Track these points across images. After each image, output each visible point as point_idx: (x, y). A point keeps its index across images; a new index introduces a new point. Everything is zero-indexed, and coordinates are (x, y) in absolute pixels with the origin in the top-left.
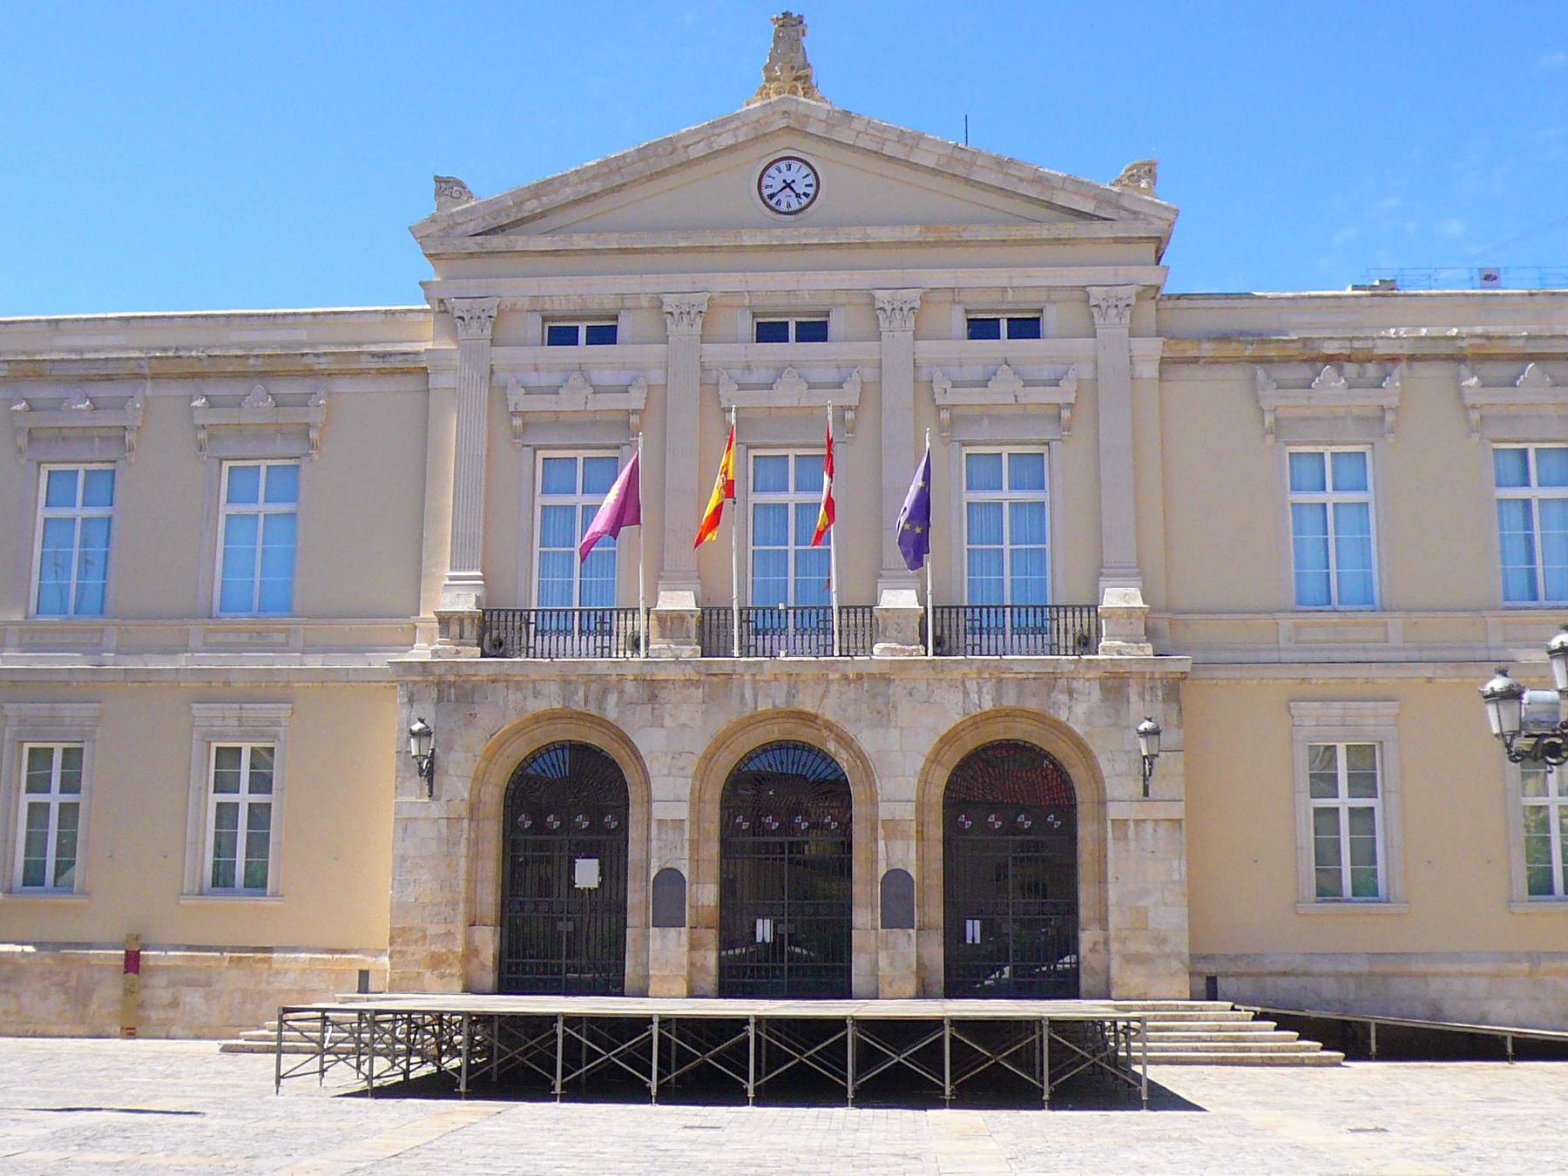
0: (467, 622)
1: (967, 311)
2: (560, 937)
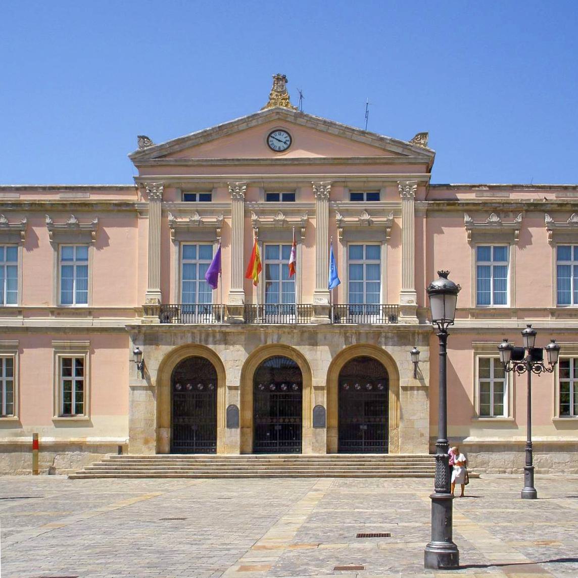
0: (155, 310)
1: (350, 191)
2: (276, 431)
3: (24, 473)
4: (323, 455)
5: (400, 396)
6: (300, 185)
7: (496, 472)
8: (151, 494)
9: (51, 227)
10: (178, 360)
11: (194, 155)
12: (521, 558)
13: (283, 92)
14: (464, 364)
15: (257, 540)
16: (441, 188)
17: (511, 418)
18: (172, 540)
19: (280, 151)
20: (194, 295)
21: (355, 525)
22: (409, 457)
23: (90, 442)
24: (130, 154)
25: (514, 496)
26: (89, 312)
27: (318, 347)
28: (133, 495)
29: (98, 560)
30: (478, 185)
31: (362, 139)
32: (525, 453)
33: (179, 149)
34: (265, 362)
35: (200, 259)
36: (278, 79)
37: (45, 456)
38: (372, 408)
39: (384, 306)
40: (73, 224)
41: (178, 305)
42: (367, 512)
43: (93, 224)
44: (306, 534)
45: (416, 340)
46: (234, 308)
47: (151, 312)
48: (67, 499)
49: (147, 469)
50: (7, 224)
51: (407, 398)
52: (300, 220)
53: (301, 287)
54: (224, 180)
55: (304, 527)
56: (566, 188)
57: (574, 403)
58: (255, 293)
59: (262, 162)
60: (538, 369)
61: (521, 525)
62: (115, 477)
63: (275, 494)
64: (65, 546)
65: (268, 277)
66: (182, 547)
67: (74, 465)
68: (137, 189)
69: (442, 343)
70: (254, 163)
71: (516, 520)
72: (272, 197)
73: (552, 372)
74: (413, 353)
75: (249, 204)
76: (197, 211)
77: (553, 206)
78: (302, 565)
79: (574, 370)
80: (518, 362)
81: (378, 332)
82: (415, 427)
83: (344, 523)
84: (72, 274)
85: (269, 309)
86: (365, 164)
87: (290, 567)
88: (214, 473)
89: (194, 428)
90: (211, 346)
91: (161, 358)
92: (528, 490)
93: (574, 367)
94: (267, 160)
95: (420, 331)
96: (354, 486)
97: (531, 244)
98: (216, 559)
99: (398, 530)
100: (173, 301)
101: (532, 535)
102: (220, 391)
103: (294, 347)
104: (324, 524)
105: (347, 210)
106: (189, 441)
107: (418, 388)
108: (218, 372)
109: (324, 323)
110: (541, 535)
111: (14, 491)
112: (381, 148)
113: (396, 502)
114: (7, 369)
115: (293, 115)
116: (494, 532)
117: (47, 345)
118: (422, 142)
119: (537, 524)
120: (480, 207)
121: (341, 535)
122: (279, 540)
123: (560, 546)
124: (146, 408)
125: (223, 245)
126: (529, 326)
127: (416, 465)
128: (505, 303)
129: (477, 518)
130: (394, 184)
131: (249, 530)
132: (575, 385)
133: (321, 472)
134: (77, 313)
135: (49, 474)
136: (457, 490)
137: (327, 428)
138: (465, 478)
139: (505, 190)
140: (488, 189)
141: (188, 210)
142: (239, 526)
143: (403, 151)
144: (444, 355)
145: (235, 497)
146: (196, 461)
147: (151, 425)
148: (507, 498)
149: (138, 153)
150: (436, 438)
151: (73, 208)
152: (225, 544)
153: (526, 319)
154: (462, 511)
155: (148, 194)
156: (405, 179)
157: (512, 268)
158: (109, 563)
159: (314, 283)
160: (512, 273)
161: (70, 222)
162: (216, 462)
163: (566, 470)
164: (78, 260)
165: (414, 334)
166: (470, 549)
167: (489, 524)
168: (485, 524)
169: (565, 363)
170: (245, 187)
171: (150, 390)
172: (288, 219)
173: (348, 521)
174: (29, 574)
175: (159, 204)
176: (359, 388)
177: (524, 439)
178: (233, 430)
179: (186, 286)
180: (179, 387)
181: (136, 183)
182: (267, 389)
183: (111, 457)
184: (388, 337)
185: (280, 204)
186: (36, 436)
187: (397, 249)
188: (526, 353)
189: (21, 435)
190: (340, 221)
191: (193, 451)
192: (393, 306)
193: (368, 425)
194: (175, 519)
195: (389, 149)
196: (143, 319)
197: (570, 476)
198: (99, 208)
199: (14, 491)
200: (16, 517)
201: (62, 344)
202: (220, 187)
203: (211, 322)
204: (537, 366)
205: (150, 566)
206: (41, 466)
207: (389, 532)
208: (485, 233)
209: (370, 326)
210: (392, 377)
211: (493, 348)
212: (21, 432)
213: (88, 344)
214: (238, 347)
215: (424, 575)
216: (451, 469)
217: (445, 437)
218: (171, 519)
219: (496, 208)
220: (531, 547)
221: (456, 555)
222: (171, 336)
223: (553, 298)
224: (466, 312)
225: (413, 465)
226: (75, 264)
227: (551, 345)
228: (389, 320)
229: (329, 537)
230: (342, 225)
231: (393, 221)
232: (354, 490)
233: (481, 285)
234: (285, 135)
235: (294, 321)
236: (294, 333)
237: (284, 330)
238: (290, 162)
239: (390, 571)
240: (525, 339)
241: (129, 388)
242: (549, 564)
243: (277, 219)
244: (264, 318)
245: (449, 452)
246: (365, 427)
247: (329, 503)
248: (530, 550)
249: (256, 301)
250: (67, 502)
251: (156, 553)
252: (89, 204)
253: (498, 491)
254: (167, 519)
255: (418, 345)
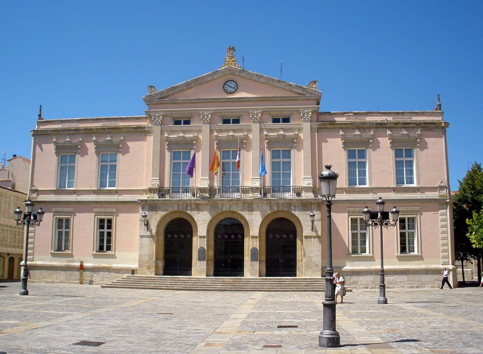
0: (155, 190)
1: (272, 117)
3: (74, 283)
4: (257, 278)
5: (304, 242)
6: (242, 114)
7: (362, 288)
8: (151, 298)
9: (96, 142)
10: (169, 220)
11: (181, 97)
12: (378, 340)
13: (233, 57)
14: (342, 221)
15: (217, 328)
16: (326, 114)
17: (371, 254)
18: (164, 326)
19: (231, 93)
20: (179, 181)
21: (277, 320)
22: (309, 279)
23: (115, 267)
24: (143, 97)
25: (374, 302)
26: (116, 192)
27: (254, 212)
28: (140, 299)
29: (118, 334)
30: (347, 112)
31: (279, 85)
32: (380, 276)
33: (172, 94)
34: (221, 222)
35: (183, 159)
36: (230, 49)
37: (87, 274)
38: (286, 249)
39: (293, 187)
40: (109, 140)
41: (170, 187)
42: (283, 313)
43: (121, 140)
44: (247, 325)
45: (313, 208)
46: (203, 189)
47: (153, 191)
48: (100, 299)
49: (149, 284)
50: (56, 142)
51: (308, 243)
52: (242, 135)
53: (243, 176)
54: (198, 112)
55: (245, 321)
56: (398, 113)
57: (409, 245)
58: (215, 180)
59: (220, 100)
60: (386, 224)
61: (378, 320)
62: (129, 288)
63: (228, 301)
64: (98, 325)
65: (223, 170)
66: (170, 331)
67: (105, 279)
68: (147, 118)
69: (328, 209)
70: (215, 101)
71: (375, 317)
72: (226, 121)
73: (395, 226)
74: (311, 216)
75: (263, 125)
76: (182, 131)
77: (391, 124)
78: (244, 344)
79: (408, 225)
80: (374, 220)
81: (290, 203)
82: (313, 260)
83: (270, 319)
84: (107, 170)
85: (224, 189)
86: (281, 100)
87: (237, 346)
88: (190, 287)
89: (178, 260)
90: (189, 212)
91: (158, 219)
92: (382, 299)
93: (408, 223)
94: (223, 99)
95: (315, 202)
96: (276, 296)
97: (379, 147)
98: (191, 338)
99: (302, 323)
100: (167, 185)
101: (385, 326)
102: (194, 239)
103: (239, 212)
104: (257, 319)
105: (271, 128)
106: (175, 268)
107: (314, 237)
108: (193, 227)
109: (257, 197)
110: (390, 326)
111: (68, 292)
112: (290, 91)
113: (301, 307)
114: (65, 225)
115: (238, 71)
116: (361, 324)
117: (90, 211)
118: (314, 86)
119: (387, 319)
120: (349, 126)
121: (267, 326)
122: (230, 329)
123: (402, 332)
124: (149, 248)
125: (197, 151)
126: (380, 198)
127: (313, 284)
128: (366, 184)
129: (351, 316)
130: (298, 112)
131: (212, 322)
132: (409, 234)
133: (255, 288)
134: (109, 192)
135: (90, 284)
136: (339, 299)
137: (259, 261)
138: (344, 292)
139: (363, 115)
140: (353, 114)
141: (176, 130)
142: (205, 319)
143: (303, 92)
144: (330, 217)
145: (202, 302)
146: (179, 280)
147: (152, 259)
148: (369, 304)
149: (148, 96)
150: (326, 267)
151: (109, 131)
152: (197, 330)
153: (378, 194)
154: (342, 312)
155: (153, 121)
156: (304, 109)
157: (369, 163)
158: (125, 337)
159: (251, 174)
160: (369, 166)
161: (107, 139)
162: (192, 281)
163: (405, 286)
164: (110, 161)
165: (311, 204)
166: (347, 335)
167: (358, 320)
168: (356, 320)
169: (402, 221)
170: (210, 115)
171: (152, 238)
172: (235, 135)
173: (272, 318)
174: (76, 338)
175: (159, 127)
176: (278, 237)
177: (379, 267)
178: (202, 262)
179: (175, 177)
180: (169, 236)
181: (146, 115)
182: (223, 237)
183: (127, 276)
184: (296, 206)
185: (231, 126)
186: (82, 262)
187: (301, 152)
188: (379, 215)
189: (73, 261)
190: (267, 135)
191: (177, 274)
192: (299, 187)
193: (284, 260)
194: (166, 314)
195: (294, 91)
196: (148, 196)
197: (407, 290)
198: (124, 130)
199: (68, 292)
200: (69, 306)
201: (99, 211)
202: (196, 116)
203: (189, 198)
204: (386, 223)
205: (151, 340)
206: (85, 280)
207: (297, 325)
208: (352, 142)
209: (285, 199)
210: (298, 230)
211: (359, 212)
212: (73, 260)
213: (115, 211)
214: (205, 212)
215: (319, 351)
216: (334, 286)
217: (331, 266)
218: (164, 314)
219: (358, 126)
220: (384, 333)
221: (338, 339)
222: (165, 206)
223: (394, 181)
224: (342, 190)
225: (312, 284)
226: (109, 164)
227: (394, 210)
228: (296, 195)
229: (260, 327)
230: (267, 138)
231: (298, 135)
232: (276, 299)
233: (351, 174)
234: (234, 83)
235: (239, 196)
236: (239, 204)
237: (233, 202)
238: (236, 100)
239: (298, 348)
240: (378, 206)
241: (139, 236)
242: (395, 343)
243: (229, 134)
244: (221, 195)
245: (333, 276)
246: (282, 261)
247: (260, 307)
248: (384, 335)
249: (216, 185)
250: (100, 300)
251: (154, 333)
252: (118, 128)
253: (364, 299)
254: (161, 314)
255: (314, 211)
